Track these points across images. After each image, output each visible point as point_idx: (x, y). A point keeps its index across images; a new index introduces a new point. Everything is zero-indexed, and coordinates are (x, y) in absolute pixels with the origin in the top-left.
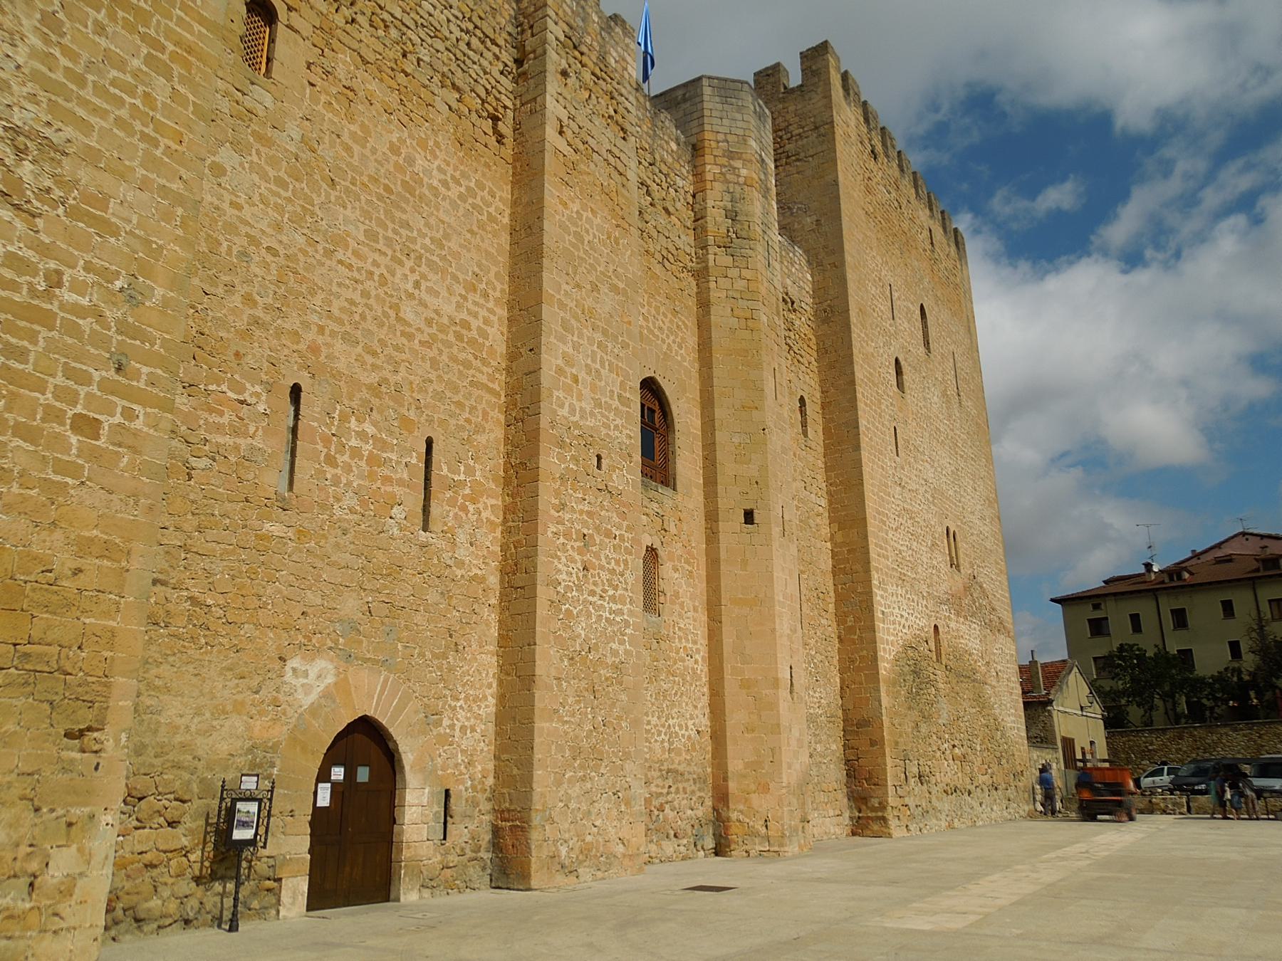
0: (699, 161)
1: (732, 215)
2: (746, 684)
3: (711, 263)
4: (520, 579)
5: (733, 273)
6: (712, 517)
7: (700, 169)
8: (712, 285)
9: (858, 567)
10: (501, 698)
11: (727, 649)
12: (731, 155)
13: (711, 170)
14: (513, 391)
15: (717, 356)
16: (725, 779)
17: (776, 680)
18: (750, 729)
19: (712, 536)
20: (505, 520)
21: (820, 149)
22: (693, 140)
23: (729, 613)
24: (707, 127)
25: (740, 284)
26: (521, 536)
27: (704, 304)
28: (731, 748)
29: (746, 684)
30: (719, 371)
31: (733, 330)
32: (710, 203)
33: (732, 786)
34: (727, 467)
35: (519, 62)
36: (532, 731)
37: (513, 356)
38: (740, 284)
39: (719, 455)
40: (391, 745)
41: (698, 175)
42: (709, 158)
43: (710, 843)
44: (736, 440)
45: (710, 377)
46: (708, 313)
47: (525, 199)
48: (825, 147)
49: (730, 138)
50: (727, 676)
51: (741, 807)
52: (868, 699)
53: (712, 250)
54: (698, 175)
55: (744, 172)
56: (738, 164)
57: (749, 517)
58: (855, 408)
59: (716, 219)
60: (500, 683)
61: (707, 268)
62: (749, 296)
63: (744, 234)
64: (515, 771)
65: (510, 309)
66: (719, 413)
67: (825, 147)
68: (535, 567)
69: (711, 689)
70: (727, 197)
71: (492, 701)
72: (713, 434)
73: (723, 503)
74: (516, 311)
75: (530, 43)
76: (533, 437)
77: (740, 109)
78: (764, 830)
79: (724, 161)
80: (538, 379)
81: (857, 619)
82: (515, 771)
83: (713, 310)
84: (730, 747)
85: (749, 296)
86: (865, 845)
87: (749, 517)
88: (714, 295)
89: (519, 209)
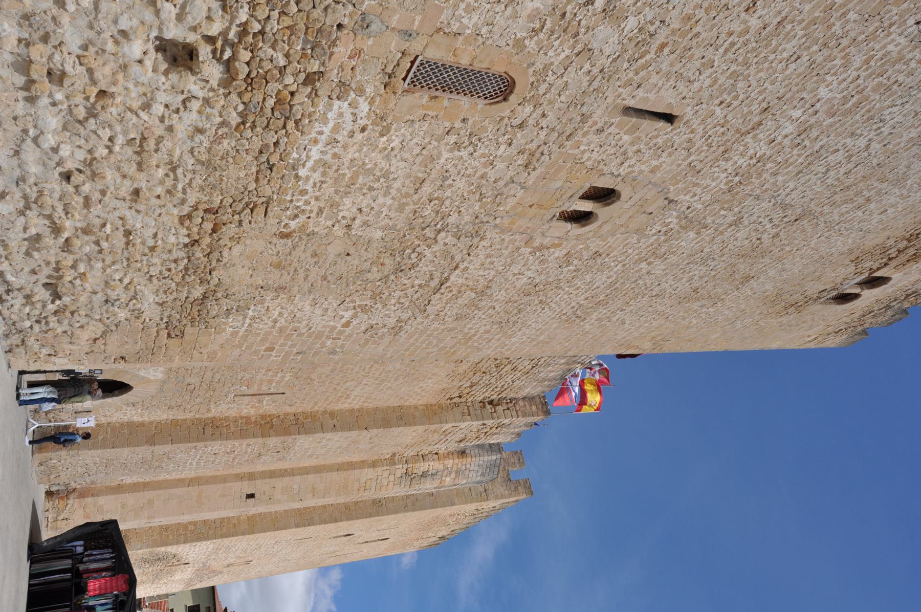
0: (455, 456)
1: (424, 475)
2: (150, 502)
3: (397, 467)
4: (209, 431)
5: (392, 478)
6: (251, 477)
7: (451, 456)
8: (385, 468)
9: (224, 530)
10: (142, 424)
11: (172, 491)
12: (458, 472)
13: (449, 463)
14: (312, 416)
15: (344, 474)
16: (93, 495)
17: (154, 518)
18: (123, 506)
19: (240, 477)
20: (242, 418)
21: (473, 493)
22: (468, 451)
23: (194, 491)
24: (474, 459)
25: (385, 482)
26: (232, 429)
27: (374, 464)
28: (111, 498)
29: (150, 502)
30: (335, 475)
31: (359, 480)
32: (431, 463)
33: (89, 500)
34: (279, 483)
35: (491, 403)
36: (123, 446)
37: (332, 414)
38: (385, 482)
39: (286, 479)
40: (117, 392)
41: (449, 455)
42: (456, 461)
43: (54, 489)
44: (295, 486)
45: (332, 471)
46: (369, 467)
47: (417, 414)
48: (474, 496)
49: (467, 472)
50: (156, 492)
51: (76, 505)
52: (142, 541)
53: (405, 466)
54: (449, 455)
55: (448, 479)
56: (453, 475)
57: (251, 496)
58: (321, 523)
59: (422, 467)
60: (151, 423)
61: (395, 464)
62: (378, 487)
63: (414, 481)
64: (100, 438)
65: (359, 410)
66: (311, 477)
67: (474, 496)
68: (215, 440)
69: (148, 483)
70: (434, 472)
71: (141, 420)
72: (300, 474)
73: (259, 482)
74: (357, 414)
75: (500, 409)
76: (286, 432)
77: (483, 475)
78: (60, 518)
79: (455, 468)
80: (318, 432)
81: (192, 532)
82: (100, 438)
83: (372, 470)
84: (112, 497)
85: (378, 487)
86: (64, 365)
87: (251, 496)
88: (379, 470)
89: (412, 411)
